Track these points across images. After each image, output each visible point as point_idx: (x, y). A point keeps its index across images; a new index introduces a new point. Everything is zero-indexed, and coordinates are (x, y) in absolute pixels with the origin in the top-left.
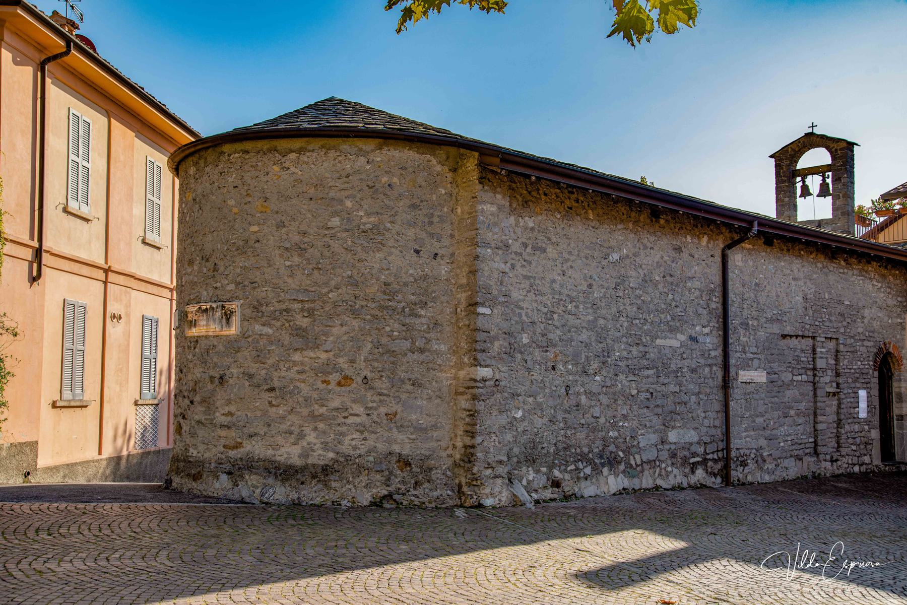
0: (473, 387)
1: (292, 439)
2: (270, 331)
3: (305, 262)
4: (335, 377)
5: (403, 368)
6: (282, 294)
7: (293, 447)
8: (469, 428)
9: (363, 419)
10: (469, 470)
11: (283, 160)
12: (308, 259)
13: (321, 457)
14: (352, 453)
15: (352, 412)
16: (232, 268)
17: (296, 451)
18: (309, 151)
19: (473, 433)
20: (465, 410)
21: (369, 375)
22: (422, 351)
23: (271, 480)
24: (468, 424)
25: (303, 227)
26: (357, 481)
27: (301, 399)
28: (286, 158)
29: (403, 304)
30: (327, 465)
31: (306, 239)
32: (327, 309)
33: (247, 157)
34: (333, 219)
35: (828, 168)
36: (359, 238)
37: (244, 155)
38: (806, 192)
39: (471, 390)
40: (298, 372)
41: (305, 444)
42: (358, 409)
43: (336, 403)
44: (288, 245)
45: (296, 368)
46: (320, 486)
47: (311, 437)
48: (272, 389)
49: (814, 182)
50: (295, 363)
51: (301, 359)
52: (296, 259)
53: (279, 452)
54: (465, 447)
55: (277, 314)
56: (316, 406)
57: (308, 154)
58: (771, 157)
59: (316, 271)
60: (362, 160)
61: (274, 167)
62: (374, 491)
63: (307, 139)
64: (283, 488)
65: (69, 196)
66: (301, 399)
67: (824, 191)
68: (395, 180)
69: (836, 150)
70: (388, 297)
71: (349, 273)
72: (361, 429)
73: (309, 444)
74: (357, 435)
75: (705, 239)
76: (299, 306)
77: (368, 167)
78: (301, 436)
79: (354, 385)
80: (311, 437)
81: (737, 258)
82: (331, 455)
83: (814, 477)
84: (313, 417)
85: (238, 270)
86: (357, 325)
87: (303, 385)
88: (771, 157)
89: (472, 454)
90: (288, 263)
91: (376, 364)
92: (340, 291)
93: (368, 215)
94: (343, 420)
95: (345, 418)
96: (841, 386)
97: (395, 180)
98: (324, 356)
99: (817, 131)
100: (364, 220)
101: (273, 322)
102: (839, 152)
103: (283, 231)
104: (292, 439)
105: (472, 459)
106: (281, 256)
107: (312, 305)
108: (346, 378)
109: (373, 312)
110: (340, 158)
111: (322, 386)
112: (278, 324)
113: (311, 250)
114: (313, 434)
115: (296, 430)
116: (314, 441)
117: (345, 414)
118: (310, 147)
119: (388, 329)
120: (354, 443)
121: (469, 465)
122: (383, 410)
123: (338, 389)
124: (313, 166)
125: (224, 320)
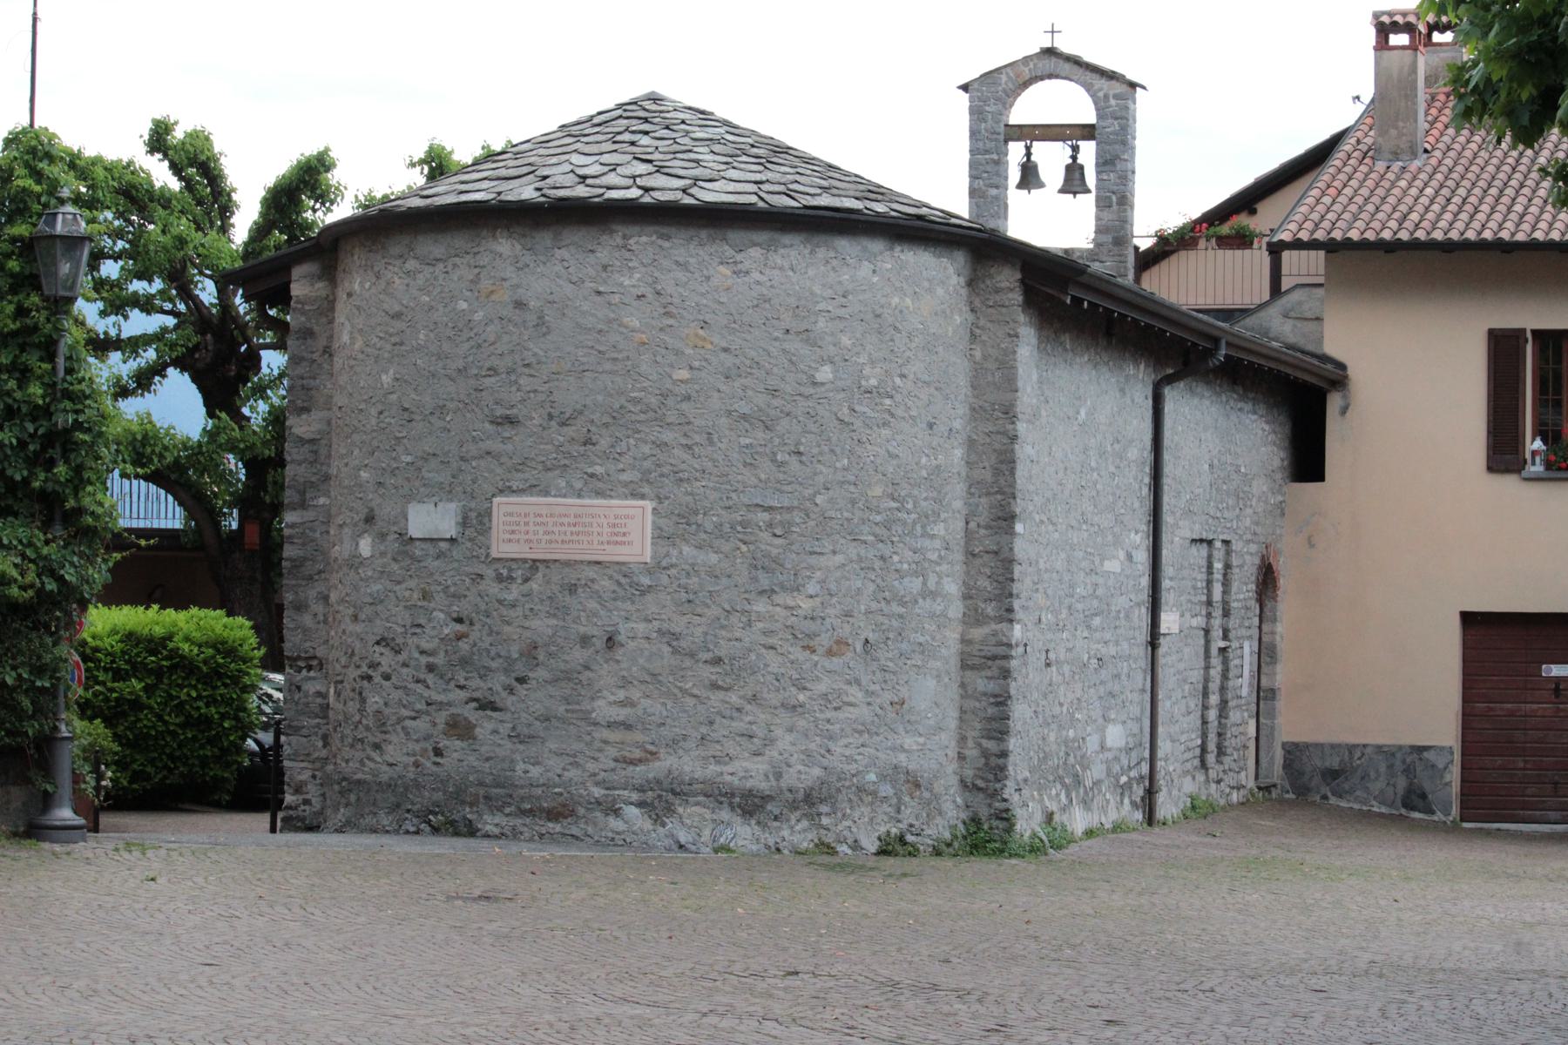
2: (714, 558)
6: (734, 495)
8: (995, 725)
9: (864, 713)
11: (739, 257)
13: (802, 775)
14: (846, 767)
16: (632, 441)
17: (758, 767)
20: (985, 694)
21: (871, 637)
23: (725, 814)
25: (773, 382)
26: (856, 814)
29: (913, 516)
31: (776, 402)
35: (1087, 132)
38: (1030, 176)
39: (998, 662)
42: (855, 694)
45: (760, 625)
46: (805, 823)
47: (785, 741)
48: (718, 661)
49: (1051, 158)
53: (729, 769)
55: (727, 528)
57: (782, 251)
58: (965, 88)
60: (866, 268)
61: (722, 269)
64: (748, 829)
67: (1073, 181)
69: (1106, 96)
72: (863, 729)
75: (1142, 367)
76: (766, 516)
77: (875, 279)
78: (769, 741)
79: (850, 655)
81: (1171, 395)
82: (817, 772)
85: (646, 449)
88: (965, 88)
96: (1232, 635)
97: (908, 301)
99: (1065, 47)
101: (717, 543)
102: (1113, 102)
103: (737, 384)
107: (787, 516)
110: (834, 262)
112: (726, 547)
115: (759, 731)
119: (896, 558)
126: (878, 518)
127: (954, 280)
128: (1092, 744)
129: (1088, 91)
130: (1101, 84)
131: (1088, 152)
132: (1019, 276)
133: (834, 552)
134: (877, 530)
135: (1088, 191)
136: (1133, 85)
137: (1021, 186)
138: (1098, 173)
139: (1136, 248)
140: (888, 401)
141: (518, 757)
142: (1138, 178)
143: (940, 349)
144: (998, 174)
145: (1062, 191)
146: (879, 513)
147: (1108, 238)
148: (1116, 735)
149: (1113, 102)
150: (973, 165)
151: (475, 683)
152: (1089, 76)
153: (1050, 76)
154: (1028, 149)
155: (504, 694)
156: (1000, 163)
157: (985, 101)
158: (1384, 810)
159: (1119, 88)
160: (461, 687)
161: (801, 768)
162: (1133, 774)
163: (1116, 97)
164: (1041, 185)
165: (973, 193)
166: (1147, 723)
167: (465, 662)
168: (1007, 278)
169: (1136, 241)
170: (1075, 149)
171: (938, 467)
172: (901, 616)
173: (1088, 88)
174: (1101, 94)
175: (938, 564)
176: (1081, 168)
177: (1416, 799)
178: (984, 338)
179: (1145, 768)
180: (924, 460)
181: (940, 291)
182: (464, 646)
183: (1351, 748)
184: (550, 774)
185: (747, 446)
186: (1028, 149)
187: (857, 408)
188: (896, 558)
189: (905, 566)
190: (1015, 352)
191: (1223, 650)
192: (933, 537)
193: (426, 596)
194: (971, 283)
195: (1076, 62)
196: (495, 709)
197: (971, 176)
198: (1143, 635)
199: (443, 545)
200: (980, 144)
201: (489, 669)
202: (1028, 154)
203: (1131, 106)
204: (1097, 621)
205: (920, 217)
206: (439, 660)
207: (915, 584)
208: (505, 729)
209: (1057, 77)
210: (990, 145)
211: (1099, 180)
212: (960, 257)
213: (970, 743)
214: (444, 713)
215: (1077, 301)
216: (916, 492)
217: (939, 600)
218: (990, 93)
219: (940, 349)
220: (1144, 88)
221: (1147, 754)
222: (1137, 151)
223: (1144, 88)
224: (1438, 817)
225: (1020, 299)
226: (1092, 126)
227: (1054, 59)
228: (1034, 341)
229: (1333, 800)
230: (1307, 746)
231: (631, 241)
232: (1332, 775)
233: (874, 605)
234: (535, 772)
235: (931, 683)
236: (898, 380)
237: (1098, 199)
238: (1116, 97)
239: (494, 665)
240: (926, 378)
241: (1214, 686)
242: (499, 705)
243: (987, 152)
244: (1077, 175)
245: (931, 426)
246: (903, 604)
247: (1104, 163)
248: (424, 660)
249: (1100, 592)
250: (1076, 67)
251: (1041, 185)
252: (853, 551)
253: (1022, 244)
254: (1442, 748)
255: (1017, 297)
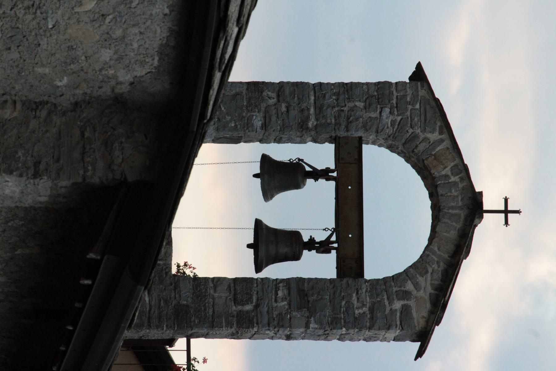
35: (351, 261)
38: (278, 177)
49: (310, 210)
58: (419, 74)
67: (270, 244)
69: (406, 295)
88: (419, 74)
102: (398, 305)
127: (125, 77)
129: (414, 266)
130: (427, 285)
131: (320, 266)
132: (131, 177)
135: (258, 269)
136: (423, 337)
137: (265, 160)
138: (287, 281)
139: (171, 342)
142: (281, 344)
143: (15, 55)
144: (283, 129)
145: (258, 224)
147: (186, 296)
149: (398, 305)
150: (299, 87)
152: (436, 269)
153: (436, 209)
154: (324, 174)
156: (302, 132)
157: (399, 107)
159: (419, 316)
163: (406, 310)
164: (268, 194)
165: (256, 88)
168: (127, 159)
169: (181, 343)
170: (323, 247)
173: (419, 267)
174: (409, 286)
176: (296, 257)
178: (33, 123)
181: (106, 55)
186: (324, 174)
190: (10, 172)
194: (119, 102)
195: (461, 247)
197: (281, 84)
200: (332, 100)
202: (317, 174)
203: (392, 334)
205: (223, 23)
209: (431, 239)
210: (330, 115)
211: (277, 282)
212: (161, 86)
215: (92, 269)
218: (411, 115)
219: (15, 55)
220: (420, 354)
222: (321, 344)
223: (420, 354)
225: (96, 180)
226: (361, 273)
227: (463, 213)
228: (28, 201)
237: (251, 280)
238: (406, 310)
243: (319, 109)
244: (284, 250)
247: (300, 288)
250: (451, 247)
251: (268, 194)
253: (185, 188)
255: (97, 175)
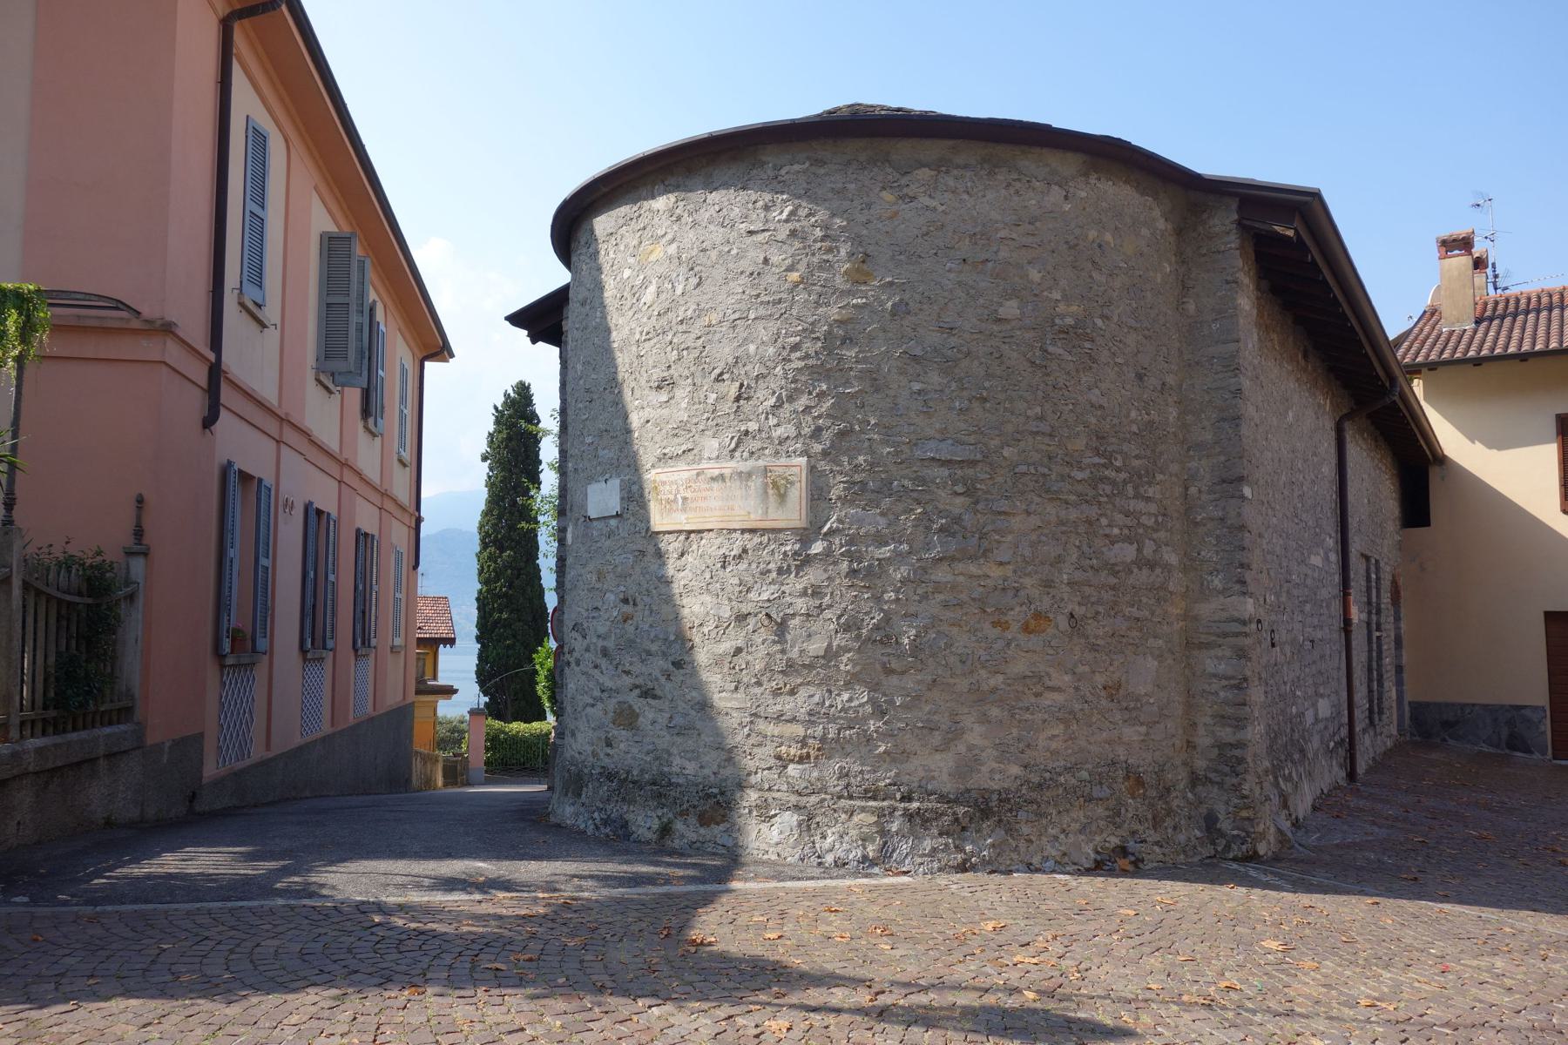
0: (1237, 635)
1: (937, 738)
3: (954, 385)
4: (1017, 615)
5: (1127, 598)
7: (938, 756)
10: (1236, 788)
11: (904, 181)
12: (961, 380)
15: (1050, 684)
18: (958, 167)
19: (1238, 719)
21: (1080, 611)
22: (1152, 565)
24: (1226, 702)
27: (952, 659)
28: (908, 177)
29: (1123, 475)
30: (1007, 791)
31: (953, 341)
32: (1000, 479)
33: (822, 171)
34: (1008, 303)
36: (1054, 343)
37: (813, 169)
40: (946, 605)
41: (962, 748)
43: (1020, 667)
44: (918, 351)
47: (975, 735)
50: (938, 588)
51: (949, 578)
52: (935, 378)
54: (1222, 746)
56: (983, 673)
59: (976, 404)
60: (1056, 193)
62: (1098, 838)
63: (951, 143)
65: (245, 277)
66: (952, 659)
68: (1108, 237)
70: (1102, 461)
71: (1038, 410)
73: (970, 748)
74: (1058, 730)
76: (945, 472)
77: (1067, 207)
78: (955, 733)
79: (1051, 631)
80: (975, 735)
82: (1015, 770)
83: (730, 751)
84: (980, 697)
86: (1053, 512)
87: (955, 630)
89: (1241, 761)
90: (916, 386)
91: (1087, 591)
92: (1022, 444)
93: (1066, 298)
94: (1033, 700)
95: (1037, 695)
97: (1108, 237)
98: (996, 572)
100: (1061, 308)
103: (905, 323)
104: (937, 738)
105: (1240, 768)
106: (902, 372)
107: (970, 472)
108: (1038, 615)
109: (1080, 488)
110: (1018, 185)
111: (993, 633)
113: (965, 363)
114: (978, 729)
116: (978, 741)
117: (1039, 688)
118: (959, 160)
119: (1104, 521)
120: (1054, 745)
121: (1235, 781)
122: (1100, 680)
123: (1022, 637)
124: (965, 197)
125: (772, 499)
126: (1079, 475)
127: (1161, 224)
128: (1309, 718)
133: (1028, 513)
134: (1080, 488)
140: (1087, 345)
141: (674, 751)
143: (1149, 294)
146: (1081, 469)
148: (1324, 708)
151: (637, 668)
155: (663, 680)
158: (1491, 750)
160: (627, 673)
161: (995, 765)
162: (1337, 738)
166: (1344, 694)
167: (631, 643)
171: (1152, 422)
172: (1113, 588)
175: (1156, 531)
177: (1517, 743)
179: (1344, 732)
180: (1133, 414)
182: (630, 628)
183: (1463, 706)
184: (706, 771)
185: (919, 392)
187: (1051, 349)
188: (1104, 521)
189: (1116, 531)
191: (1378, 638)
192: (1148, 499)
193: (601, 576)
194: (1179, 232)
196: (655, 697)
198: (1338, 623)
199: (613, 522)
201: (649, 653)
204: (1308, 607)
206: (610, 644)
207: (1128, 552)
208: (663, 719)
213: (1201, 731)
214: (614, 701)
216: (1125, 447)
217: (1158, 571)
219: (1149, 294)
221: (1345, 720)
224: (1537, 756)
229: (1451, 742)
230: (1428, 704)
231: (783, 172)
232: (1447, 725)
233: (1079, 576)
234: (691, 767)
235: (1152, 664)
236: (1099, 322)
239: (654, 648)
240: (1132, 323)
241: (1374, 665)
242: (658, 692)
245: (1140, 377)
246: (1115, 574)
248: (600, 643)
249: (1309, 582)
252: (1051, 510)
254: (1536, 708)
